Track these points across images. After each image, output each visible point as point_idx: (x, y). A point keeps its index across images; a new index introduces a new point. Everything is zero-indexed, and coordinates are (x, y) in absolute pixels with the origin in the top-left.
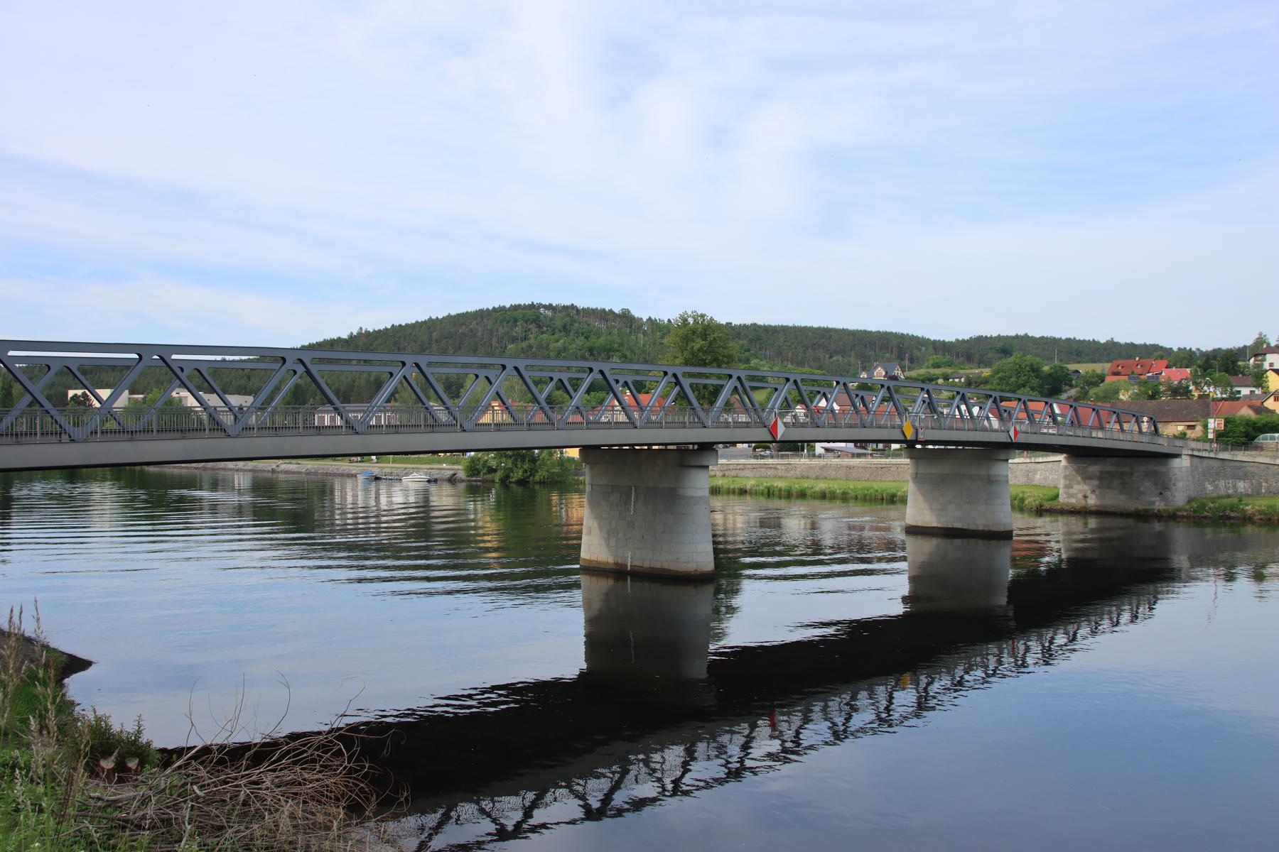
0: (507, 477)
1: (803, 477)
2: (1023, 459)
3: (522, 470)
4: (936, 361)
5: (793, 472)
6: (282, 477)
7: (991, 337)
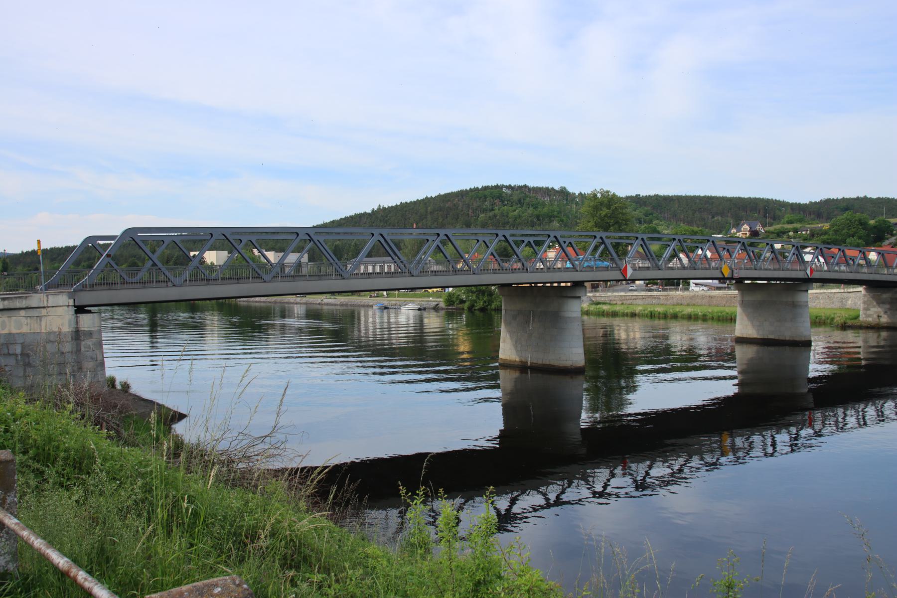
0: (473, 306)
1: (678, 304)
2: (838, 290)
3: (483, 301)
4: (790, 219)
5: (671, 301)
6: (325, 307)
7: (837, 199)
